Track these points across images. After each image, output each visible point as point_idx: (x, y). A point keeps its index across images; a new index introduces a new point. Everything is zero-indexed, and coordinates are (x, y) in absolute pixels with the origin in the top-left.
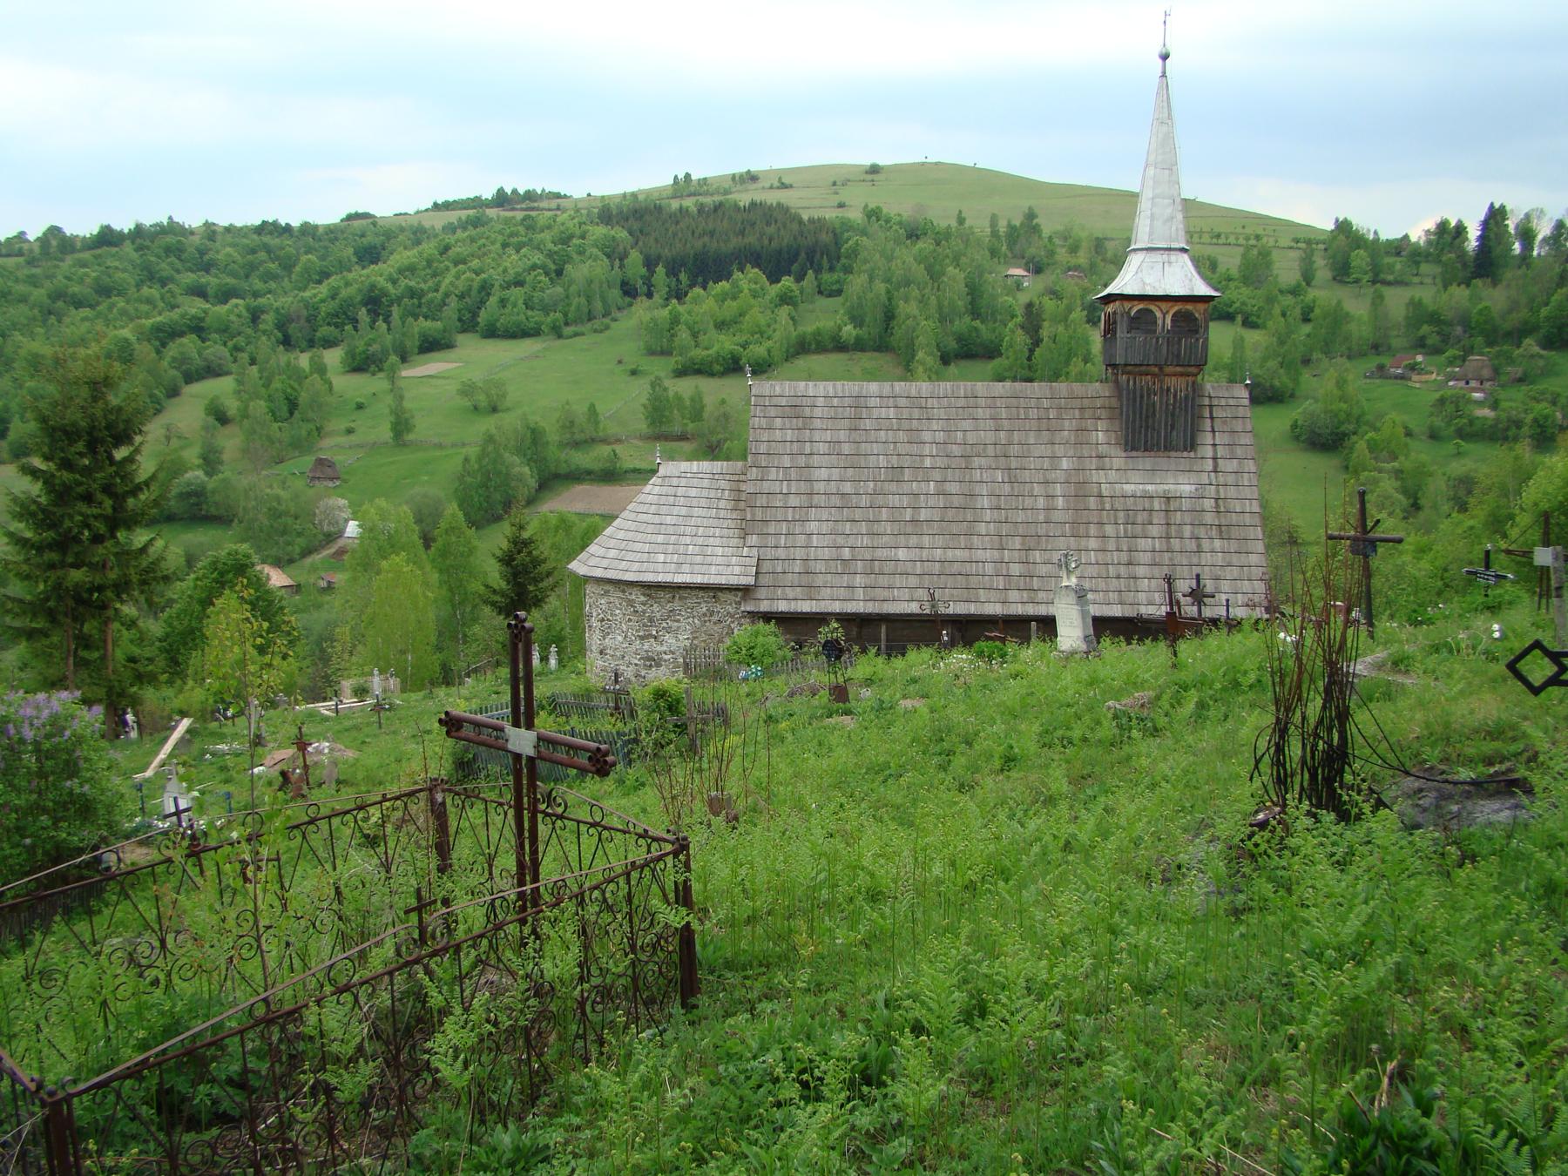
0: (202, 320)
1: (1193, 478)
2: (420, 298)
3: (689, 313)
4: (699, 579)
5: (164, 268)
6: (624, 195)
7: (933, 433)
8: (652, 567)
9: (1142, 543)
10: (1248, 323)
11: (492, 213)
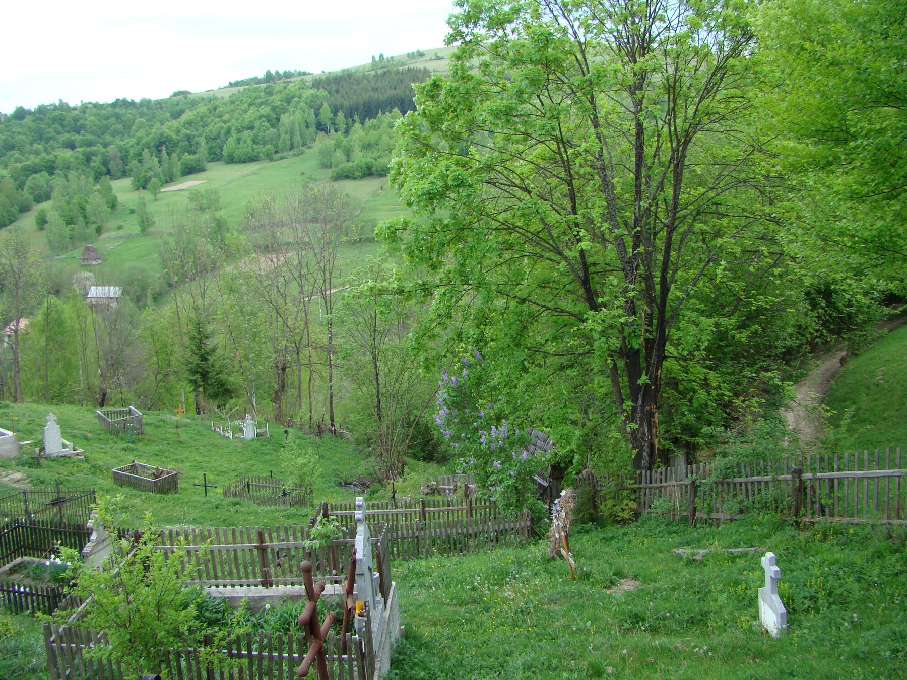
0: (54, 162)
5: (51, 132)
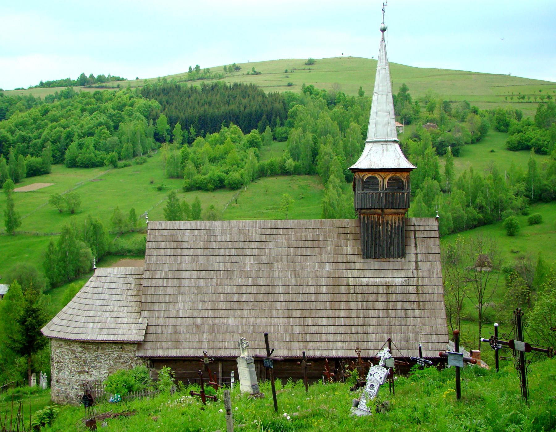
1: (403, 274)
2: (29, 142)
4: (111, 338)
6: (159, 79)
7: (252, 249)
8: (85, 330)
9: (372, 313)
10: (540, 151)
11: (77, 89)
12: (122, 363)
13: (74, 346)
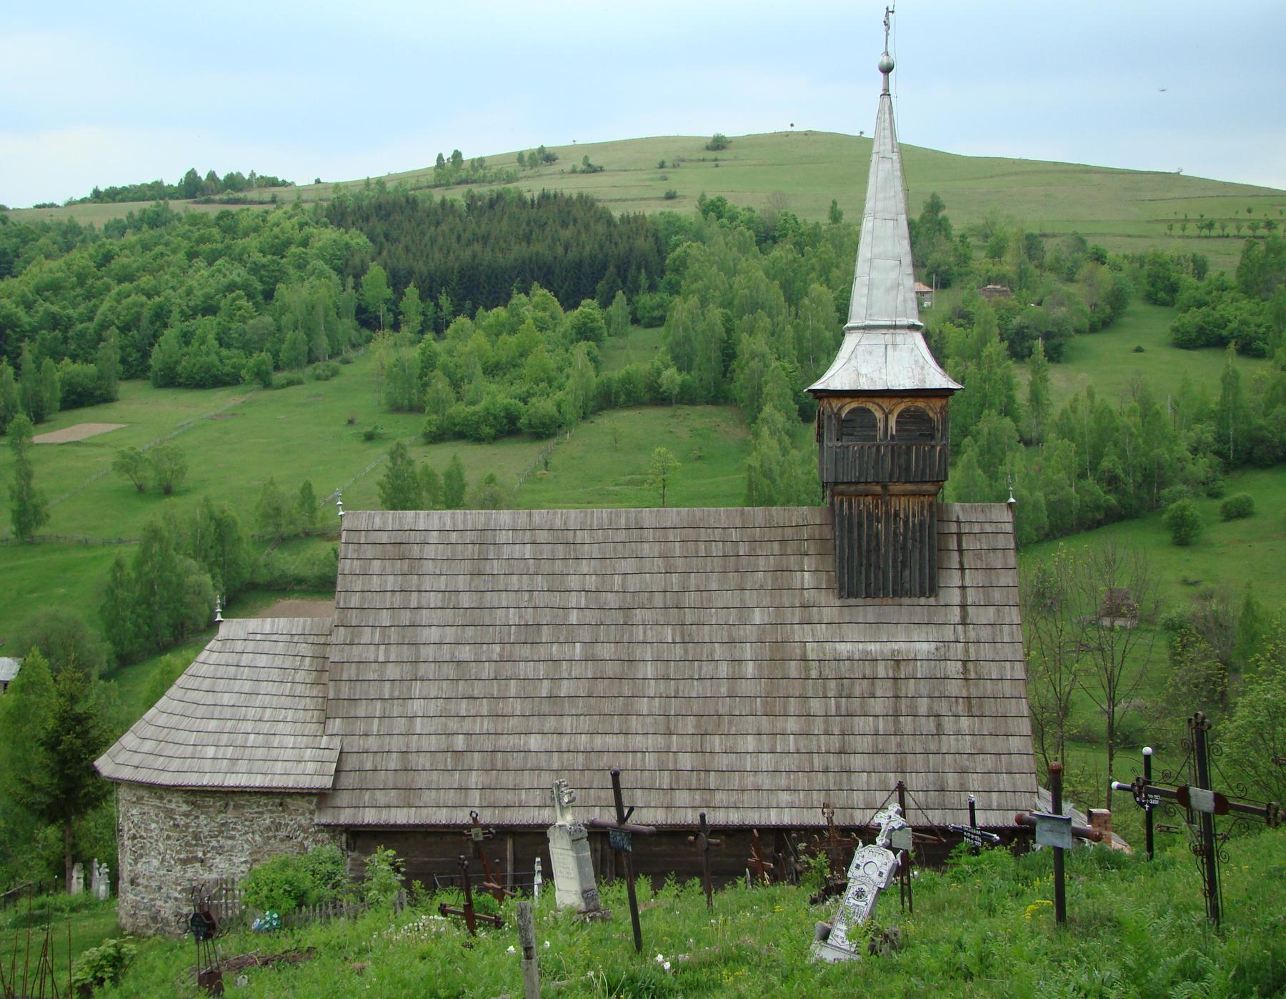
1: (933, 633)
2: (67, 329)
3: (450, 353)
4: (258, 781)
6: (367, 182)
7: (582, 576)
8: (196, 764)
9: (861, 724)
11: (177, 206)
12: (282, 840)
13: (170, 801)
